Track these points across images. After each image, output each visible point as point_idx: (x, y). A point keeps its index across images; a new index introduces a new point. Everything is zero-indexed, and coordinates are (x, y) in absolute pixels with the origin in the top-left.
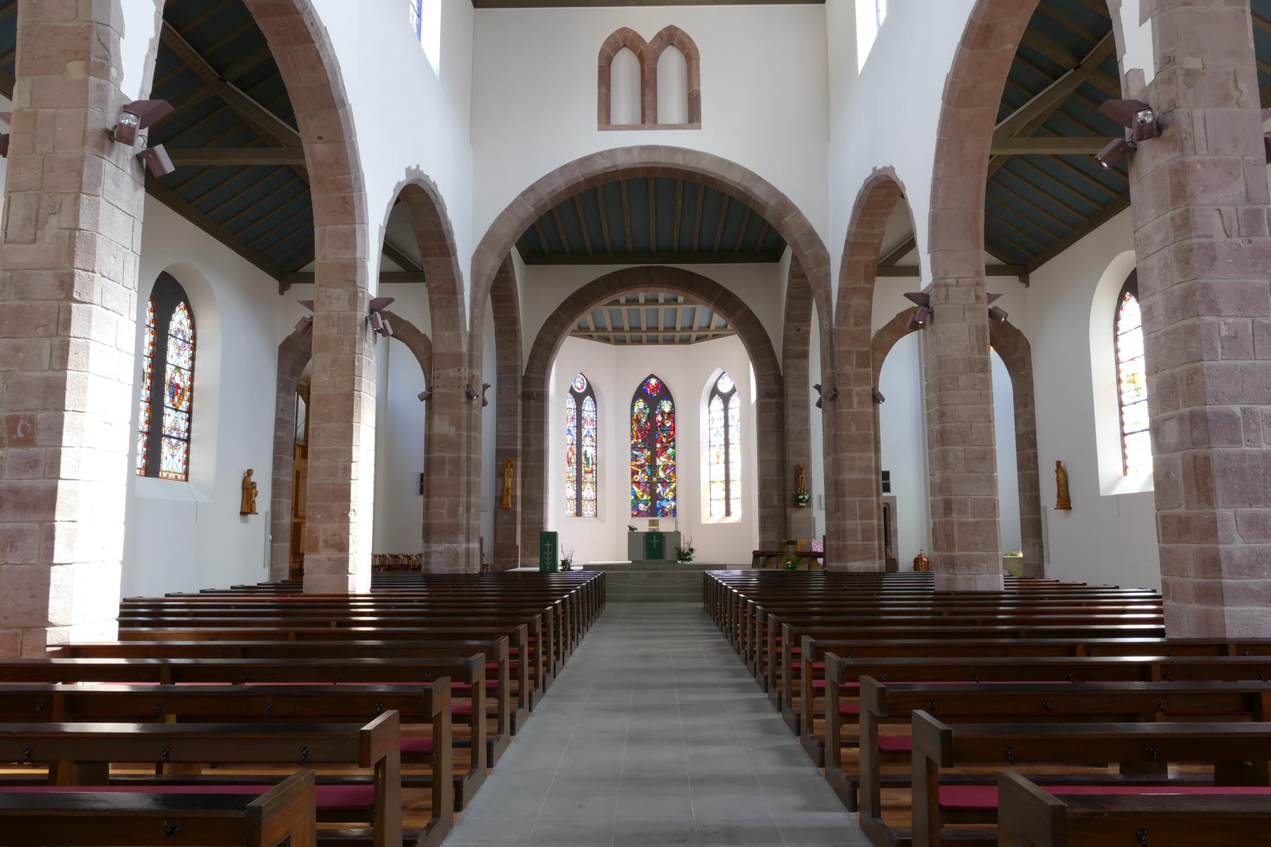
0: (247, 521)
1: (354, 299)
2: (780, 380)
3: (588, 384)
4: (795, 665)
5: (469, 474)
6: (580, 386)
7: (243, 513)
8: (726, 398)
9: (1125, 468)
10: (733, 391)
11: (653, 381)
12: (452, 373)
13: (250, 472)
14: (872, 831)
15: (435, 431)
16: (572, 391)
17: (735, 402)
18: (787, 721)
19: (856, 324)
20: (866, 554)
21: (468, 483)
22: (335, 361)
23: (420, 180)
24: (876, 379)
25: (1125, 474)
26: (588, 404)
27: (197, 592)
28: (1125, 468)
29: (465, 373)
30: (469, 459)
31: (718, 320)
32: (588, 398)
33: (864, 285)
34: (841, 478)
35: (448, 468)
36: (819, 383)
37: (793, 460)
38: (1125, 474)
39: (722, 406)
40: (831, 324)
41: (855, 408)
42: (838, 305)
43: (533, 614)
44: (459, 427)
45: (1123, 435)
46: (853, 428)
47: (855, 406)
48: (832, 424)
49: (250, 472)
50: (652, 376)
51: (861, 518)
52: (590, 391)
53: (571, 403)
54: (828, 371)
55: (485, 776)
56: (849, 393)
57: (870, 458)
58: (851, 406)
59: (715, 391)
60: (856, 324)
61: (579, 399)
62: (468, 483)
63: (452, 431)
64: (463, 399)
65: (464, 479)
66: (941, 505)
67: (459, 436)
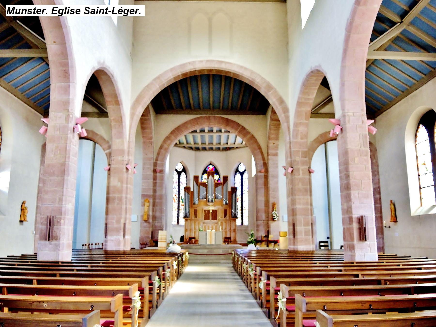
0: (22, 225)
1: (68, 118)
2: (265, 165)
3: (184, 167)
4: (268, 289)
5: (126, 204)
6: (180, 168)
7: (21, 221)
8: (242, 174)
9: (421, 204)
10: (245, 171)
11: (211, 167)
12: (120, 158)
13: (24, 203)
14: (273, 324)
15: (112, 184)
16: (176, 170)
17: (246, 175)
18: (258, 303)
19: (302, 139)
20: (306, 242)
21: (126, 209)
22: (57, 147)
23: (105, 68)
24: (310, 163)
25: (421, 206)
26: (183, 175)
27: (6, 257)
28: (421, 204)
29: (126, 158)
30: (126, 198)
31: (239, 140)
32: (183, 173)
33: (304, 121)
34: (295, 207)
35: (116, 201)
36: (285, 165)
37: (271, 200)
38: (421, 206)
39: (240, 178)
40: (290, 139)
41: (301, 176)
42: (294, 130)
43: (159, 267)
44: (122, 183)
45: (420, 188)
46: (300, 185)
47: (301, 175)
48: (291, 183)
49: (24, 203)
50: (211, 164)
51: (304, 226)
52: (184, 170)
53: (176, 175)
54: (289, 159)
55: (156, 310)
56: (298, 169)
57: (308, 199)
58: (299, 175)
59: (237, 171)
60: (302, 139)
61: (179, 173)
62: (126, 209)
63: (119, 184)
64: (125, 170)
65: (124, 206)
66: (348, 220)
67: (122, 187)
